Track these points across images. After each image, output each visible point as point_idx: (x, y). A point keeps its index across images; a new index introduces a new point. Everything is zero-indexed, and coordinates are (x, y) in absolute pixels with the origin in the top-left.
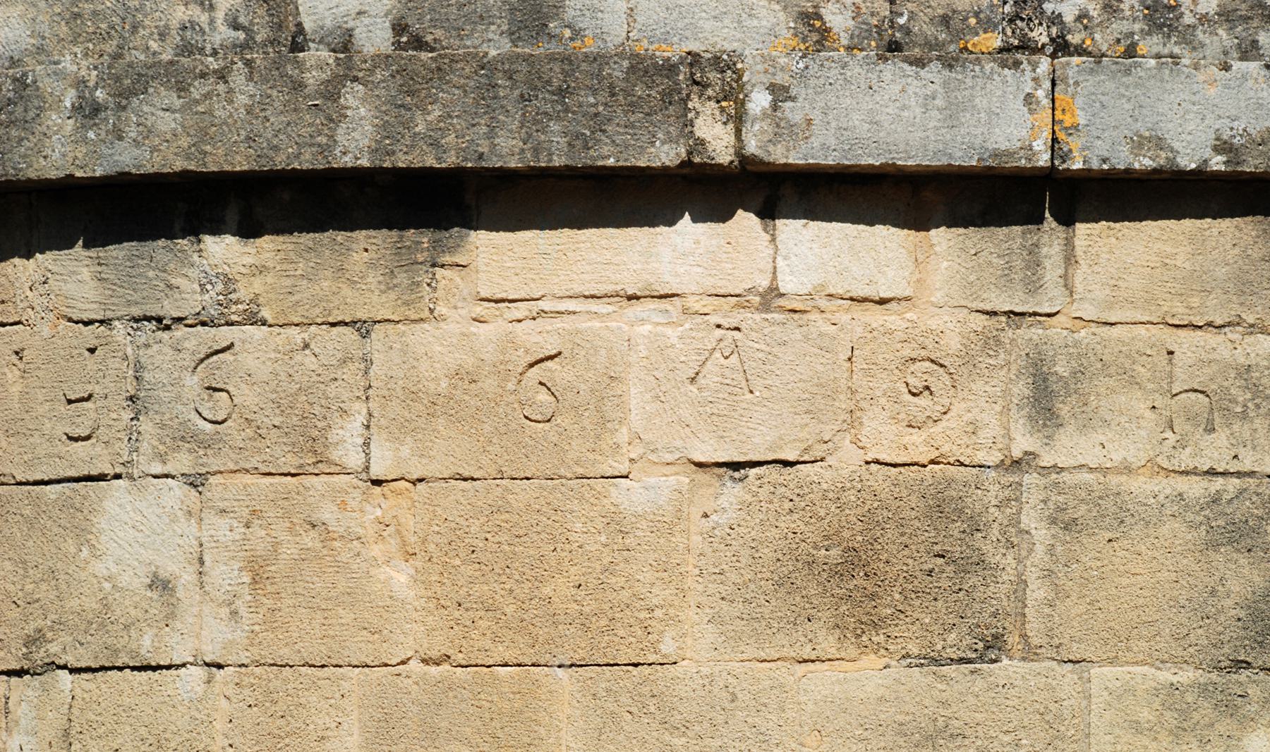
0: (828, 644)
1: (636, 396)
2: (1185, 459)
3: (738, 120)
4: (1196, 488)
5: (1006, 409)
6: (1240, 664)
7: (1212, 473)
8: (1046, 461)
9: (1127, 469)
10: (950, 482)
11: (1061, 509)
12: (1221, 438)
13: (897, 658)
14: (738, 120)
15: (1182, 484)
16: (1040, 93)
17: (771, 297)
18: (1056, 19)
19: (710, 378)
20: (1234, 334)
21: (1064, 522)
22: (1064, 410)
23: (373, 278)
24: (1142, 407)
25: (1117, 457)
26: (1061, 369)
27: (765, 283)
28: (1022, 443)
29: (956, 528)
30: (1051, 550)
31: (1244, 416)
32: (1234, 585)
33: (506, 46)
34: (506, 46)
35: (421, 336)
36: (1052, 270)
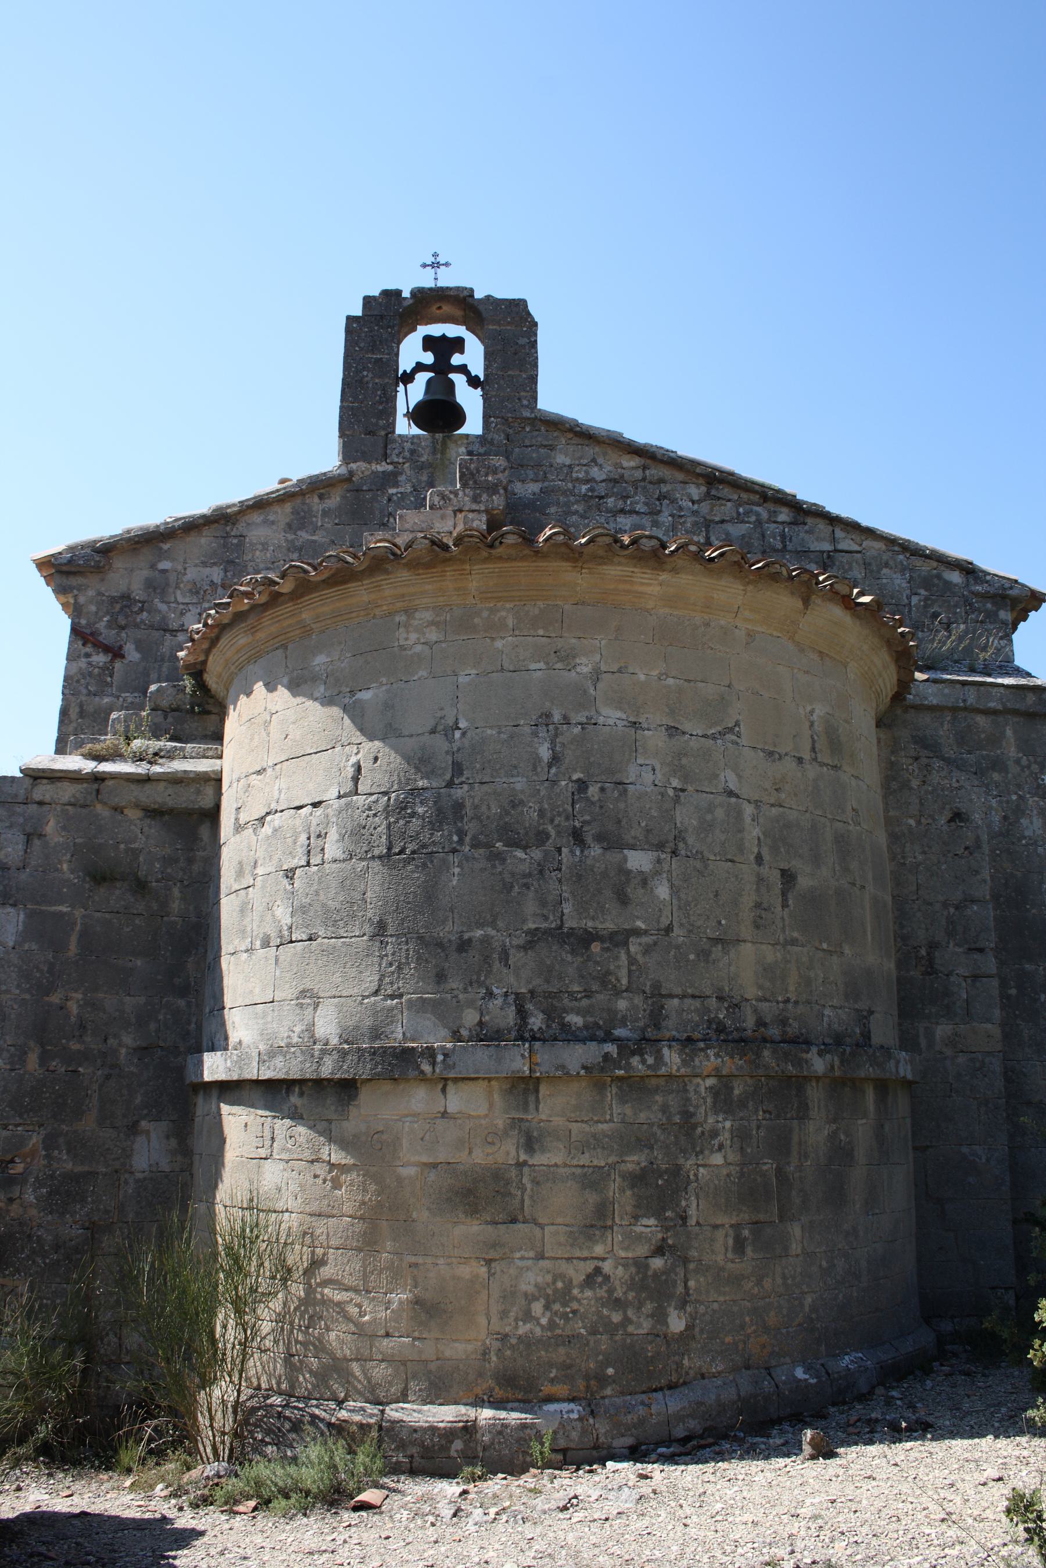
0: (462, 1216)
1: (405, 1143)
2: (575, 1162)
3: (434, 1064)
4: (579, 1171)
5: (517, 1148)
6: (592, 1226)
7: (584, 1166)
8: (530, 1163)
9: (556, 1165)
10: (500, 1169)
11: (535, 1177)
12: (587, 1155)
13: (537, 1231)
14: (434, 1064)
15: (574, 1170)
16: (526, 1054)
17: (444, 1114)
18: (532, 1030)
19: (427, 1137)
20: (591, 1123)
21: (536, 1182)
22: (536, 1147)
23: (333, 1108)
24: (561, 1146)
25: (553, 1163)
26: (535, 1134)
27: (442, 1110)
28: (523, 1157)
29: (502, 1183)
30: (532, 1190)
31: (594, 1148)
32: (591, 1201)
33: (304, 616)
34: (304, 616)
35: (345, 1124)
36: (532, 1106)
